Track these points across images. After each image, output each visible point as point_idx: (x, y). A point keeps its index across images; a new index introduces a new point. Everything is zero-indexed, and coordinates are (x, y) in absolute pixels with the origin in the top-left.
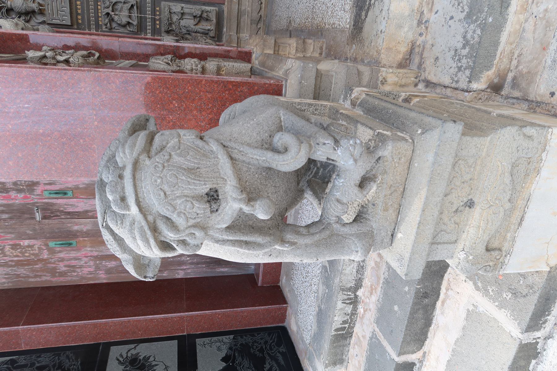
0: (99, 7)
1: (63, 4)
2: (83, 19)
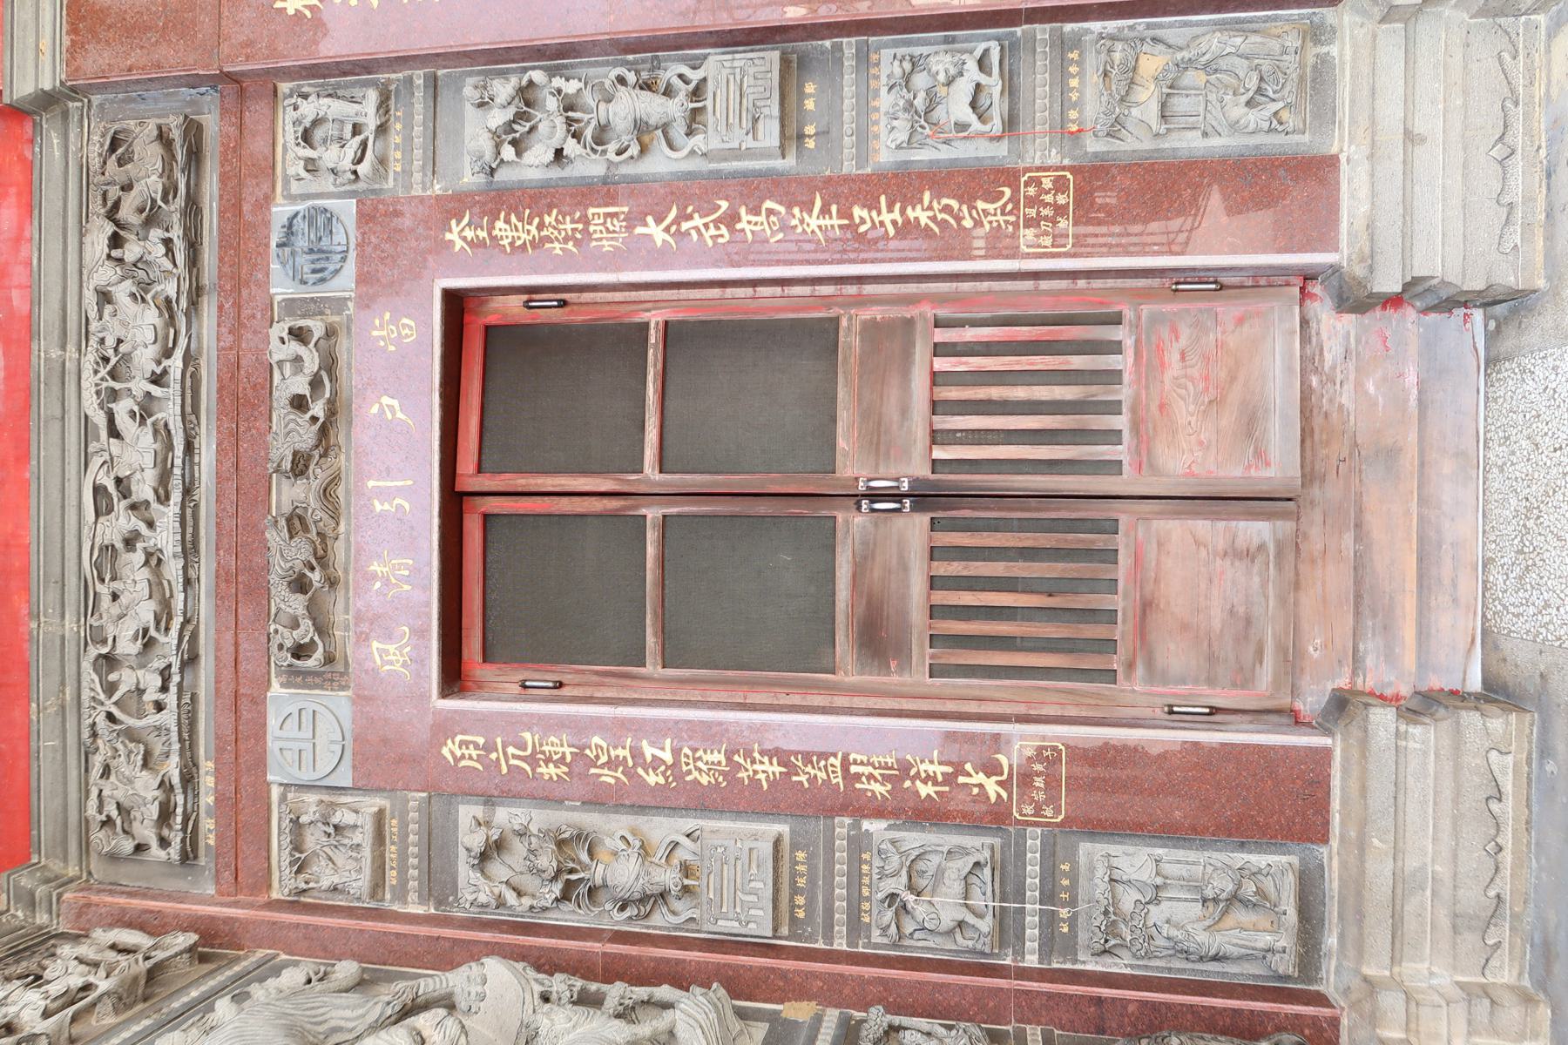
0: (865, 868)
1: (754, 870)
2: (810, 906)
